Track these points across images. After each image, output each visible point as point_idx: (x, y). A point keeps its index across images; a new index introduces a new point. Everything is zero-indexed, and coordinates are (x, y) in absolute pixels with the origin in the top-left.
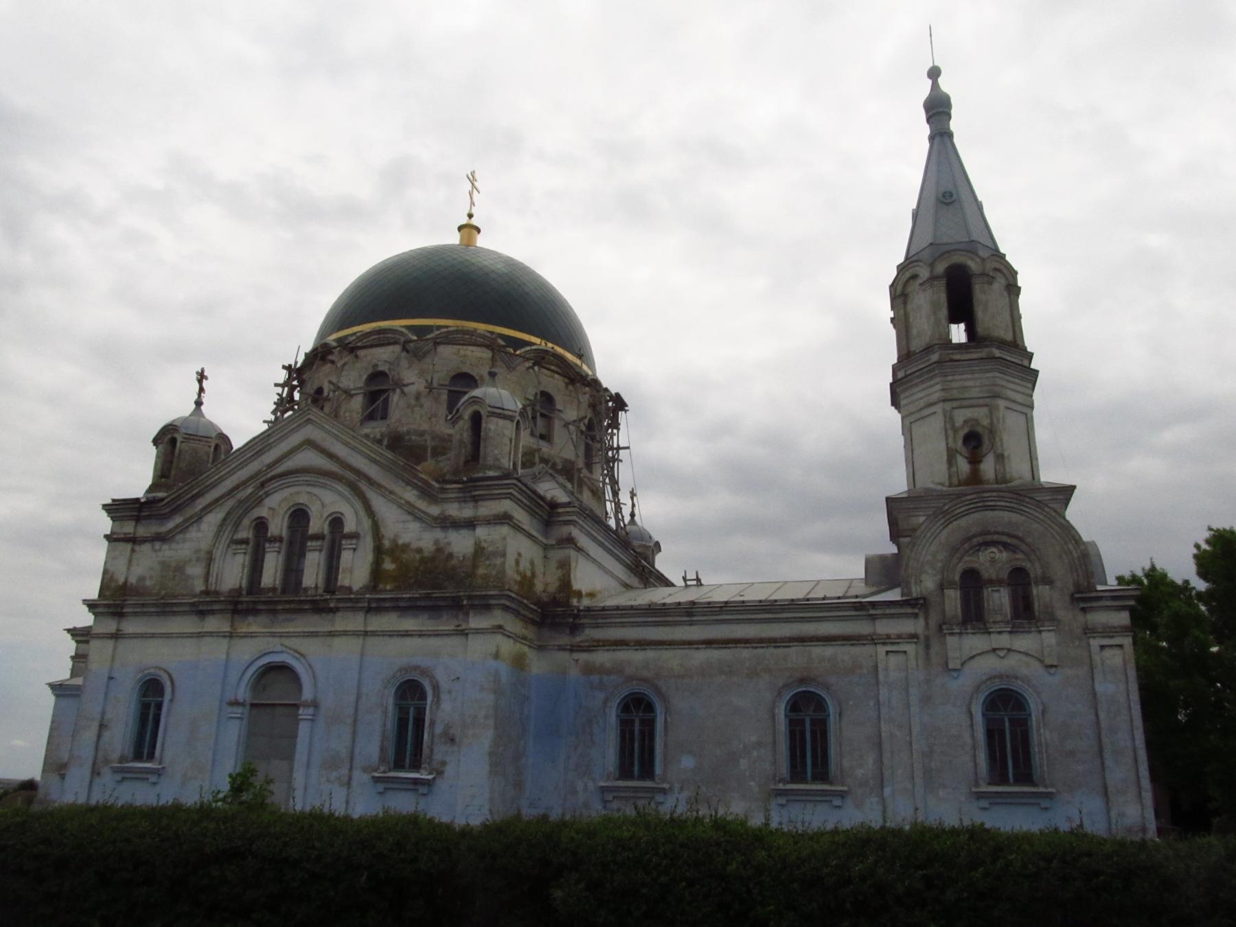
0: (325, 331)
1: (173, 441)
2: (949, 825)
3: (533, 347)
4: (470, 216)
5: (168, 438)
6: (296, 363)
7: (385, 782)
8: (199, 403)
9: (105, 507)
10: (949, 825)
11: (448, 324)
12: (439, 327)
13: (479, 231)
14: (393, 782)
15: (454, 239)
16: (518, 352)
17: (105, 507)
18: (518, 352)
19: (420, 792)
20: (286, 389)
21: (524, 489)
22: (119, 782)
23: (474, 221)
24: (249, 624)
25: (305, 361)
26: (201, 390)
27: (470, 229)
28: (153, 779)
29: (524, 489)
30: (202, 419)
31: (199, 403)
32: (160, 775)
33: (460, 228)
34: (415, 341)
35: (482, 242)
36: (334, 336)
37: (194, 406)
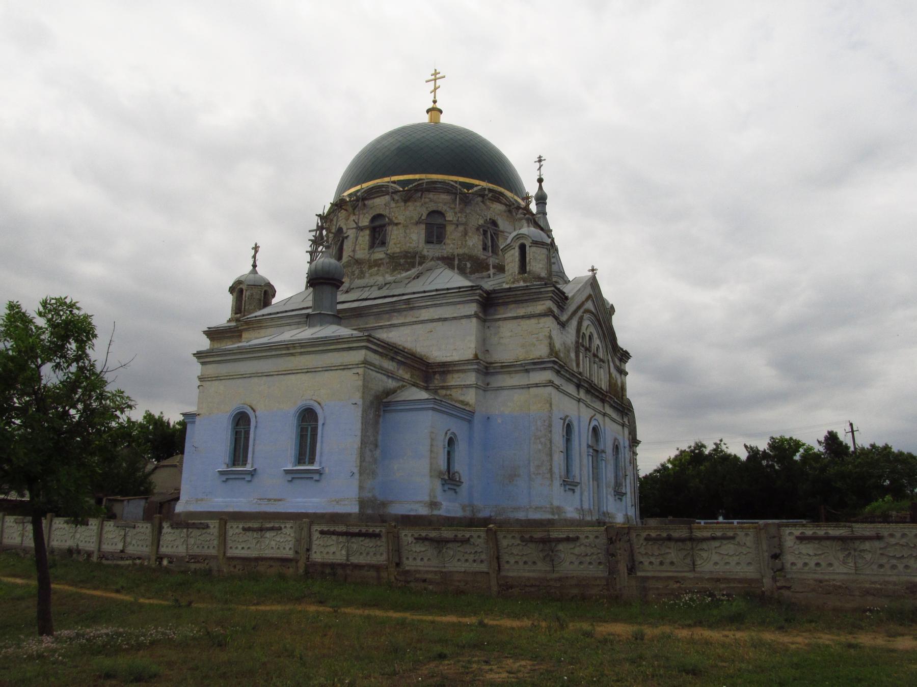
0: (343, 187)
1: (241, 291)
2: (819, 442)
3: (475, 189)
4: (435, 102)
5: (237, 289)
6: (324, 213)
7: (292, 473)
8: (254, 266)
9: (205, 332)
10: (819, 442)
11: (422, 178)
12: (415, 180)
13: (441, 112)
14: (296, 473)
15: (425, 119)
16: (470, 191)
17: (205, 332)
18: (470, 191)
19: (247, 479)
20: (318, 232)
21: (379, 342)
22: (290, 481)
23: (438, 105)
24: (406, 316)
25: (330, 208)
26: (254, 257)
27: (434, 111)
28: (316, 477)
29: (379, 342)
30: (256, 275)
31: (254, 266)
32: (252, 475)
33: (428, 111)
34: (401, 191)
35: (444, 119)
36: (346, 194)
37: (252, 268)
